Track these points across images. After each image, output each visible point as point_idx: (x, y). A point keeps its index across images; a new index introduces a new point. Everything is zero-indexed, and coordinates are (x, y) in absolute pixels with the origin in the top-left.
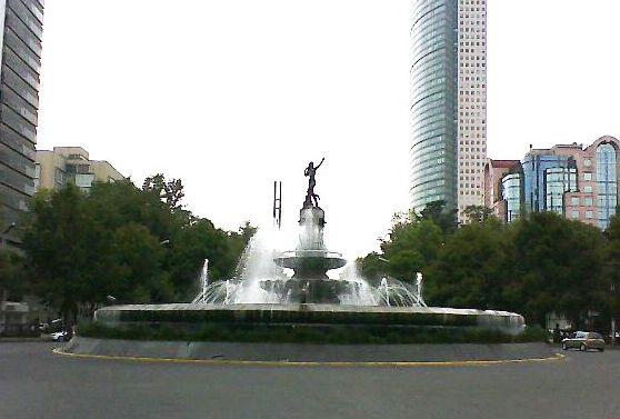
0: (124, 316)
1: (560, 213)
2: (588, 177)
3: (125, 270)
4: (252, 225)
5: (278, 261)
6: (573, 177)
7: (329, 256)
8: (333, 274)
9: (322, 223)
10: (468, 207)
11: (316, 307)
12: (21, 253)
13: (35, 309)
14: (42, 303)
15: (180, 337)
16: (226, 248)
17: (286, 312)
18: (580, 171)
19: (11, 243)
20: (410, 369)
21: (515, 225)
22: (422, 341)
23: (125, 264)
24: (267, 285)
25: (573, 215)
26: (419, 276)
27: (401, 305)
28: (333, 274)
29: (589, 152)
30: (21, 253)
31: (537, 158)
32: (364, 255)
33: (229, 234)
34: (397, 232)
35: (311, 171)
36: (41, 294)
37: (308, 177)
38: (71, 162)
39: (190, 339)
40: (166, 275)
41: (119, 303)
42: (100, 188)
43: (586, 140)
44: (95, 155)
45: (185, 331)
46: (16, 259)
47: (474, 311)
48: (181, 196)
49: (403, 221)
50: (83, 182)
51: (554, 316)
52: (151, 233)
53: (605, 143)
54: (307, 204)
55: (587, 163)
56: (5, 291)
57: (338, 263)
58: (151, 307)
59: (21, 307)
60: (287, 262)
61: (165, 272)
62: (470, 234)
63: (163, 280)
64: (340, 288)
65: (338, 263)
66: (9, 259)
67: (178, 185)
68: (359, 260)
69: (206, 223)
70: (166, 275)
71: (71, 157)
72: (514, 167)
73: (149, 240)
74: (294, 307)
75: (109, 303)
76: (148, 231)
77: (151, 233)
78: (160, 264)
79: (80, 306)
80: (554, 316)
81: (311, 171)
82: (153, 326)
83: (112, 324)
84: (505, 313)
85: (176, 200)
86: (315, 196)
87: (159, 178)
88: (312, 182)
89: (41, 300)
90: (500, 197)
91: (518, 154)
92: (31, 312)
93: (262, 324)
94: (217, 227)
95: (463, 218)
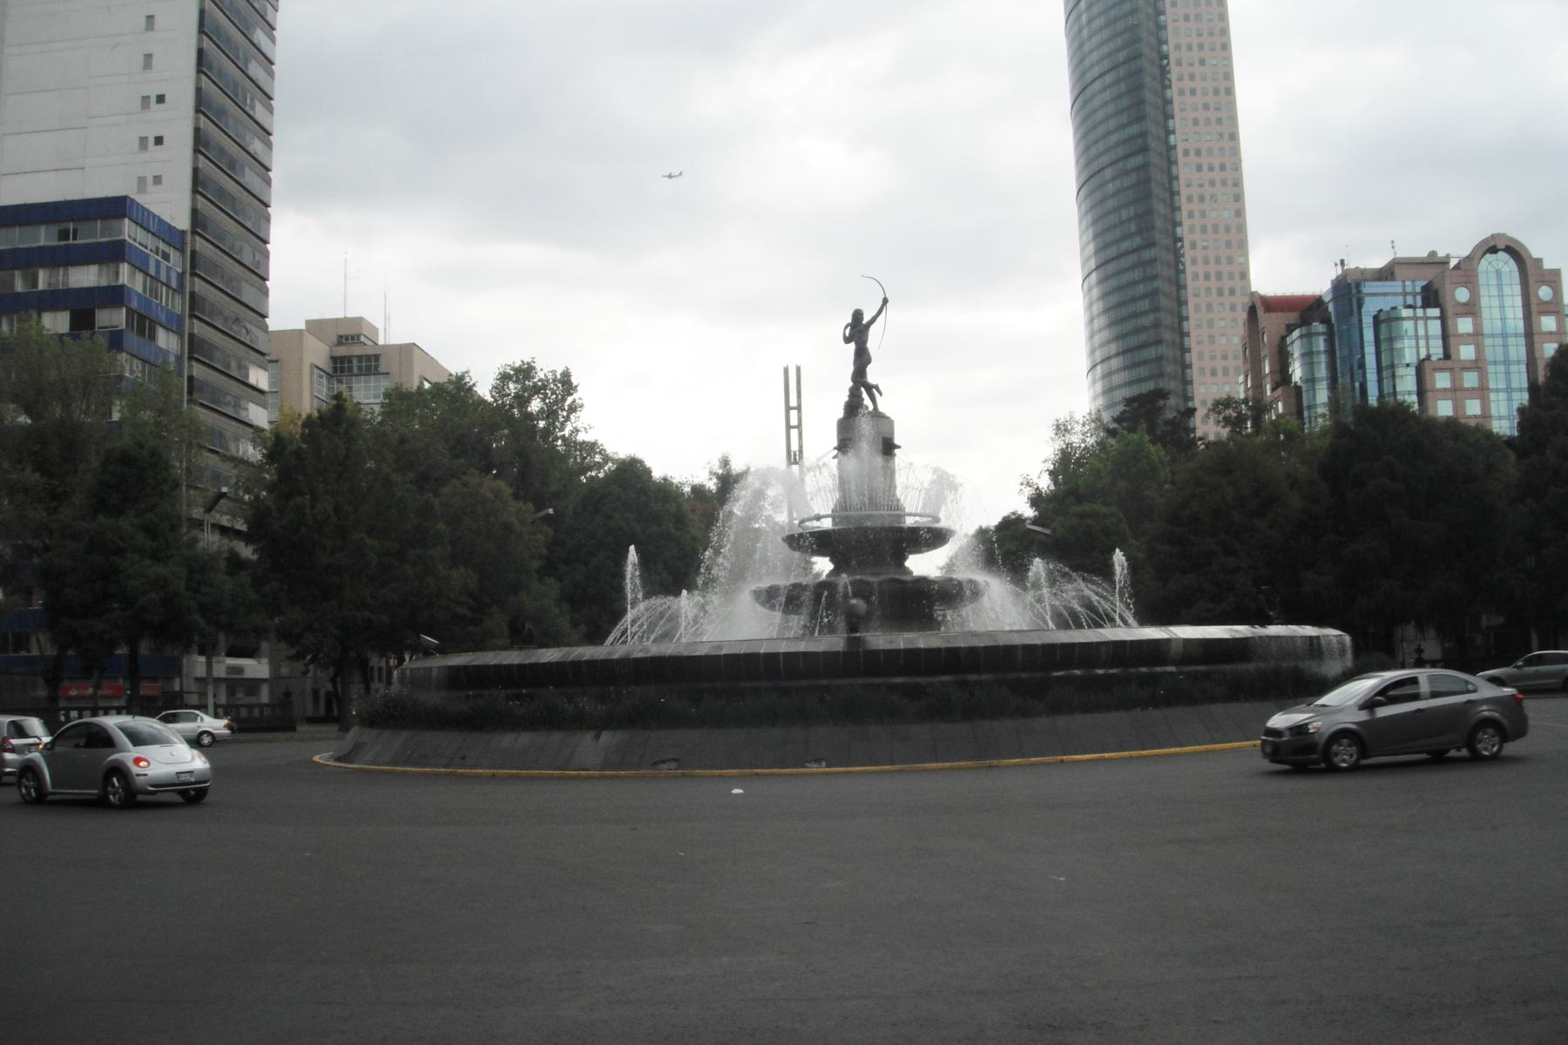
0: (458, 679)
1: (1416, 407)
2: (1464, 325)
3: (461, 577)
4: (737, 467)
5: (794, 541)
6: (1435, 327)
7: (910, 522)
8: (923, 565)
9: (888, 448)
10: (1217, 403)
11: (880, 640)
12: (247, 552)
13: (285, 671)
14: (298, 657)
15: (579, 722)
16: (680, 520)
17: (938, 650)
18: (1450, 312)
19: (224, 531)
20: (428, 378)
21: (1324, 432)
22: (1127, 704)
23: (707, 608)
24: (768, 597)
25: (1444, 409)
26: (1119, 557)
27: (1079, 626)
28: (923, 565)
29: (1466, 270)
30: (247, 552)
31: (1348, 288)
32: (993, 521)
33: (687, 489)
34: (1065, 465)
35: (858, 331)
36: (288, 636)
37: (852, 346)
38: (342, 351)
39: (600, 725)
40: (552, 588)
41: (443, 651)
42: (401, 401)
43: (1456, 248)
44: (391, 334)
45: (585, 703)
46: (235, 562)
47: (1242, 631)
48: (573, 409)
49: (1075, 439)
50: (367, 396)
51: (1410, 631)
52: (516, 496)
53: (1493, 250)
54: (853, 406)
55: (1462, 295)
56: (222, 637)
57: (935, 537)
58: (513, 657)
59: (256, 668)
60: (822, 542)
61: (550, 581)
62: (1224, 459)
63: (544, 595)
64: (947, 593)
65: (935, 537)
66: (223, 565)
67: (566, 383)
68: (982, 533)
69: (631, 472)
70: (552, 588)
71: (342, 340)
72: (1306, 311)
73: (515, 511)
74: (833, 642)
75: (427, 652)
76: (508, 491)
77: (516, 496)
78: (536, 564)
79: (376, 661)
80: (1410, 631)
81: (858, 331)
82: (518, 697)
83: (433, 698)
84: (1309, 631)
85: (567, 419)
86: (870, 388)
87: (525, 372)
88: (862, 359)
89: (293, 652)
90: (1283, 378)
91: (1316, 282)
92: (276, 678)
93: (765, 684)
94: (657, 474)
95: (1207, 428)
